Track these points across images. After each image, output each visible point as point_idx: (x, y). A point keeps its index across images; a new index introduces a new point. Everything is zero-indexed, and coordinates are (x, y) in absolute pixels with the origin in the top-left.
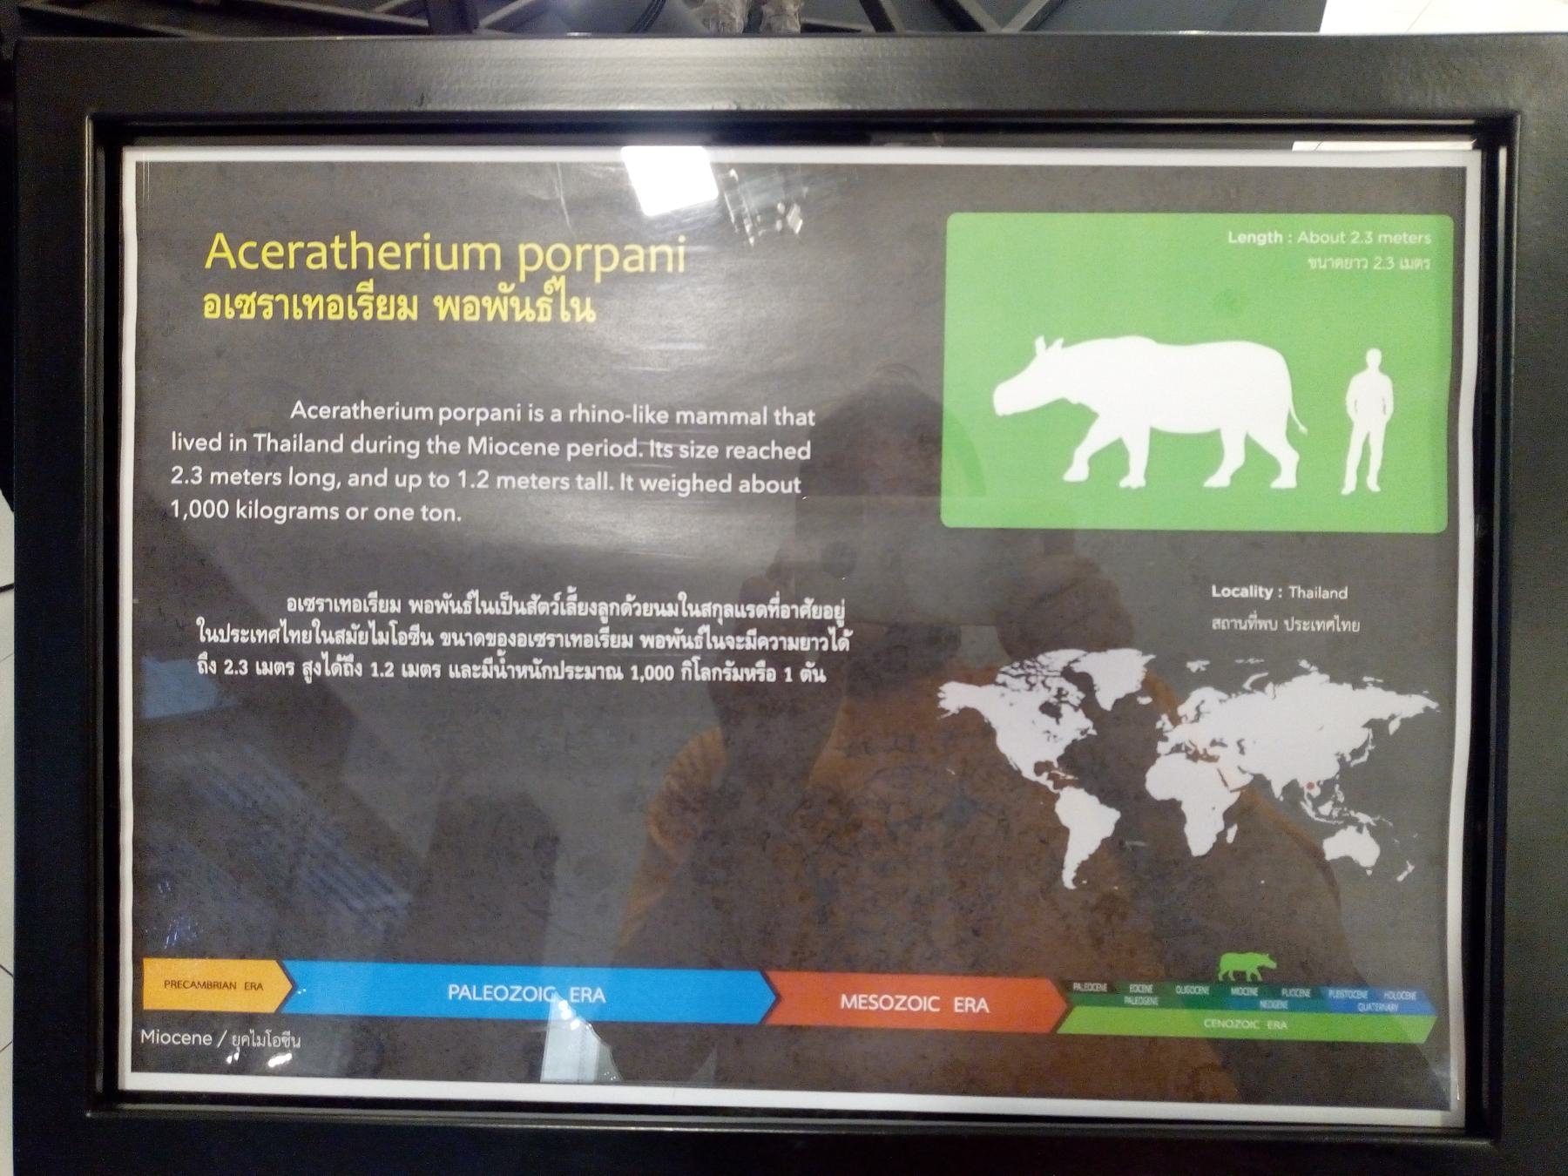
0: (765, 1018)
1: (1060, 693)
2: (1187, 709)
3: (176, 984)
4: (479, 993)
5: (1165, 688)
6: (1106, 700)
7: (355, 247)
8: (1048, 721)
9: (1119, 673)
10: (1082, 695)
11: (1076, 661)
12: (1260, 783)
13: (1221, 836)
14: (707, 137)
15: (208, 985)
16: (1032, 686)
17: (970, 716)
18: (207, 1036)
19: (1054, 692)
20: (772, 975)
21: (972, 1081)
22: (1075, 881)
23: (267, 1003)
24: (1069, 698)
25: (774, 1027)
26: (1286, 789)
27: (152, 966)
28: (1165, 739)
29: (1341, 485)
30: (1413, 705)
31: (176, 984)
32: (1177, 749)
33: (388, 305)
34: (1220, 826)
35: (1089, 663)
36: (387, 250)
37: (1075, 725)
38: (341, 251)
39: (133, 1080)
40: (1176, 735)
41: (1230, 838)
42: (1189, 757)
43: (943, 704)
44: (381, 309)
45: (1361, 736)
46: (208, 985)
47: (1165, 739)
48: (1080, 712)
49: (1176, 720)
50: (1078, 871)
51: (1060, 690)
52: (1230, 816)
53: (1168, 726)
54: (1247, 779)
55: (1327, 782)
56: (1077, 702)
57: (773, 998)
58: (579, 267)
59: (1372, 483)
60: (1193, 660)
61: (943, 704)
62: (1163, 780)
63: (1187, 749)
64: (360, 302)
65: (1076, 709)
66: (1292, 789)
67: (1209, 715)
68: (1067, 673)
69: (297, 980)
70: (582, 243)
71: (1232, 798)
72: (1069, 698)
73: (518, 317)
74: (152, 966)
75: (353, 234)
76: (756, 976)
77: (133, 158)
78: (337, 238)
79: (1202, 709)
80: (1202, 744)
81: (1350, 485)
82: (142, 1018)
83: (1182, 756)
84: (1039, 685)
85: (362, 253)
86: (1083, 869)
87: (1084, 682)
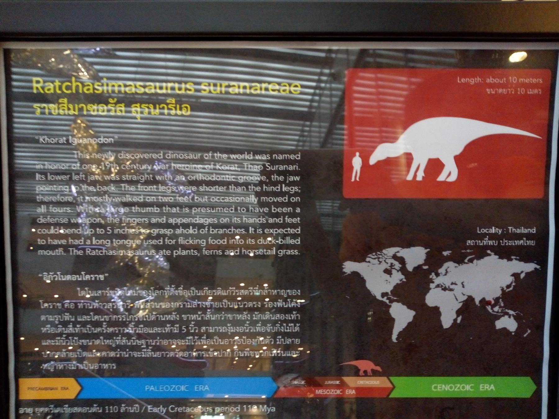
1: (392, 265)
2: (442, 271)
4: (158, 389)
6: (410, 267)
8: (387, 276)
10: (400, 266)
11: (398, 252)
12: (470, 299)
13: (455, 320)
15: (46, 389)
16: (381, 262)
17: (356, 275)
19: (389, 265)
20: (79, 379)
22: (397, 339)
23: (71, 395)
25: (277, 398)
28: (433, 282)
30: (530, 267)
32: (438, 286)
34: (455, 316)
35: (404, 253)
37: (397, 277)
42: (442, 289)
43: (344, 270)
45: (510, 280)
46: (46, 389)
47: (433, 282)
48: (400, 273)
51: (392, 264)
52: (459, 312)
54: (465, 298)
56: (398, 268)
59: (358, 179)
60: (445, 251)
61: (344, 270)
63: (442, 286)
65: (398, 271)
68: (395, 257)
79: (448, 270)
81: (353, 180)
83: (440, 289)
84: (383, 262)
86: (400, 334)
87: (402, 261)
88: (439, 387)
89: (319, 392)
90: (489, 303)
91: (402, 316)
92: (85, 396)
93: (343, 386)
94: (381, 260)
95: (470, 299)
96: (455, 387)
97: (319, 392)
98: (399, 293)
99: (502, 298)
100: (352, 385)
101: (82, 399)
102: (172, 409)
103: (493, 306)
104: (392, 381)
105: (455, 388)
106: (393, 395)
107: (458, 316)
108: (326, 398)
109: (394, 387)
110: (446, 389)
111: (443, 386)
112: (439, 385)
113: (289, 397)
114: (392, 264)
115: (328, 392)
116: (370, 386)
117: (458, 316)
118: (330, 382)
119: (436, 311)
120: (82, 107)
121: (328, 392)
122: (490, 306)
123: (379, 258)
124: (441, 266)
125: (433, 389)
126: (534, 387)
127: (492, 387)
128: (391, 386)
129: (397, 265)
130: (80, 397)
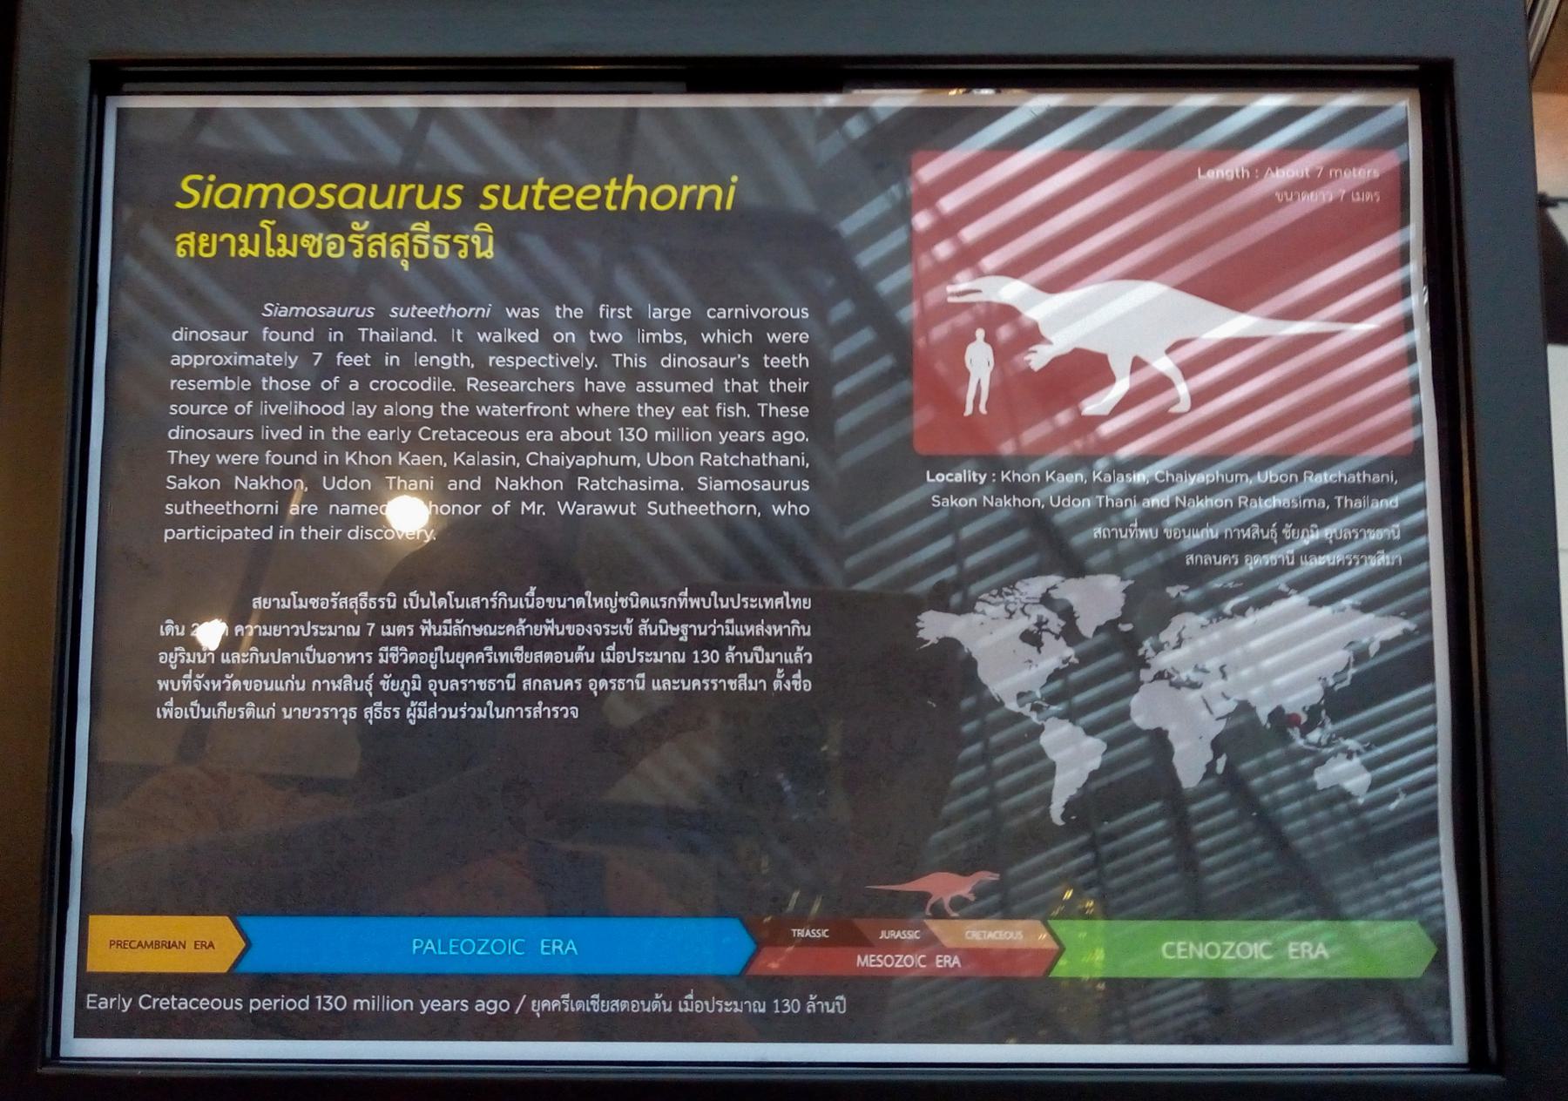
0: (235, 965)
1: (1040, 623)
2: (1168, 636)
3: (120, 944)
4: (445, 947)
5: (1147, 612)
6: (1087, 627)
7: (629, 189)
8: (1029, 650)
9: (1099, 598)
10: (1063, 623)
11: (1054, 587)
12: (1245, 707)
13: (1211, 766)
14: (683, 85)
15: (156, 945)
16: (1012, 614)
17: (950, 646)
18: (140, 1002)
19: (1034, 620)
20: (244, 921)
21: (322, 1028)
22: (1063, 816)
23: (218, 962)
24: (1049, 626)
25: (757, 978)
26: (1271, 716)
27: (95, 921)
28: (1148, 666)
29: (964, 409)
30: (1395, 628)
31: (120, 944)
32: (1160, 676)
33: (210, 241)
34: (1209, 756)
35: (1072, 591)
36: (559, 193)
37: (1057, 654)
38: (616, 192)
39: (77, 1047)
40: (1165, 660)
41: (1220, 768)
42: (1171, 684)
43: (921, 634)
44: (203, 244)
45: (1342, 656)
46: (156, 945)
47: (1148, 666)
48: (1062, 641)
49: (1158, 649)
50: (1067, 806)
51: (1040, 618)
52: (1218, 746)
53: (1150, 653)
54: (1230, 706)
55: (1312, 707)
56: (1057, 630)
57: (243, 945)
58: (682, 207)
59: (982, 409)
60: (1173, 585)
61: (921, 634)
62: (1145, 710)
63: (1170, 676)
64: (415, 240)
65: (1057, 637)
66: (1277, 715)
67: (1188, 644)
68: (1046, 600)
69: (251, 936)
70: (407, 184)
71: (1220, 726)
72: (1049, 626)
73: (479, 255)
74: (95, 921)
75: (630, 178)
76: (225, 921)
77: (114, 104)
78: (613, 181)
79: (1184, 634)
80: (1186, 674)
81: (969, 411)
82: (87, 982)
83: (1166, 683)
84: (1019, 612)
85: (636, 196)
86: (1069, 806)
87: (1068, 614)
88: (1180, 950)
89: (866, 961)
90: (1293, 720)
91: (1073, 756)
92: (258, 963)
93: (929, 943)
94: (1012, 608)
95: (1245, 707)
96: (1223, 949)
97: (866, 961)
98: (1062, 693)
99: (1324, 707)
100: (947, 941)
101: (246, 974)
102: (146, 1002)
103: (1306, 730)
104: (245, 927)
105: (478, 948)
106: (1063, 968)
107: (1217, 755)
108: (892, 978)
109: (1061, 951)
110: (1200, 955)
111: (1192, 946)
112: (1180, 943)
113: (785, 973)
114: (1040, 618)
115: (909, 961)
116: (1006, 946)
117: (1217, 755)
118: (895, 935)
119: (1159, 741)
120: (228, 240)
121: (889, 961)
122: (1297, 730)
123: (1007, 603)
124: (1164, 624)
125: (1166, 956)
126: (1428, 952)
127: (572, 946)
128: (1053, 945)
129: (1056, 623)
130: (242, 968)
